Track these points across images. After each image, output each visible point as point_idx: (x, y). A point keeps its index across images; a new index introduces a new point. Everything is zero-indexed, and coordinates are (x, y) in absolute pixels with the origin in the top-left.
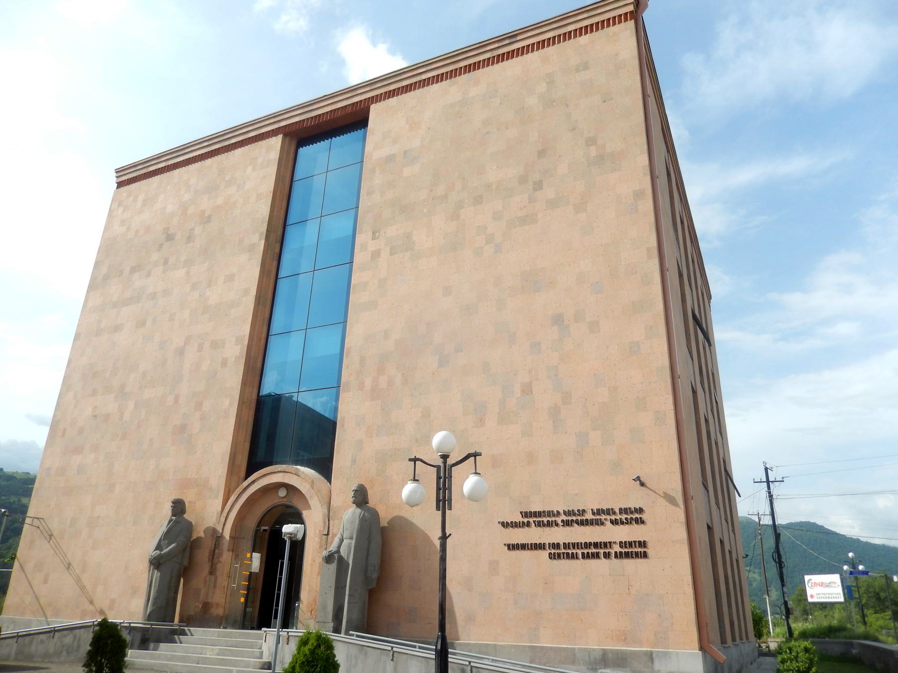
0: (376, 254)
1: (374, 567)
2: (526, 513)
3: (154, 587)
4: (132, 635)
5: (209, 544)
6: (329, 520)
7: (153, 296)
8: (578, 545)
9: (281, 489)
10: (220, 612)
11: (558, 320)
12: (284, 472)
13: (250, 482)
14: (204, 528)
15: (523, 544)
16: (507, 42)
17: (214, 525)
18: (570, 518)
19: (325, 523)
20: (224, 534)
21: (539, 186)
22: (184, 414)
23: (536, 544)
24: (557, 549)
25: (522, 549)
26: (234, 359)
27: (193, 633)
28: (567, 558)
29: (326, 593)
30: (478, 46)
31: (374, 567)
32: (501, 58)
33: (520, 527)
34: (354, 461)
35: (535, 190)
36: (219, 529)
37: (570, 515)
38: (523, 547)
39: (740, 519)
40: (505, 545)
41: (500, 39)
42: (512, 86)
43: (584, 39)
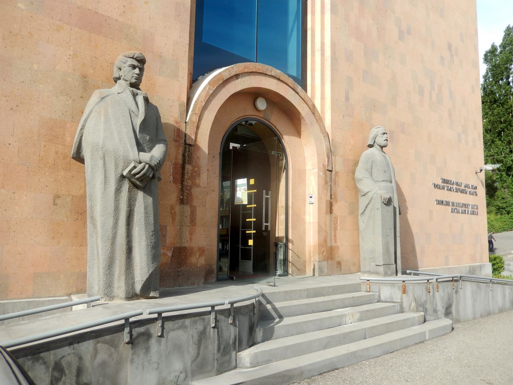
12: (279, 79)
36: (190, 132)
39: (236, 180)
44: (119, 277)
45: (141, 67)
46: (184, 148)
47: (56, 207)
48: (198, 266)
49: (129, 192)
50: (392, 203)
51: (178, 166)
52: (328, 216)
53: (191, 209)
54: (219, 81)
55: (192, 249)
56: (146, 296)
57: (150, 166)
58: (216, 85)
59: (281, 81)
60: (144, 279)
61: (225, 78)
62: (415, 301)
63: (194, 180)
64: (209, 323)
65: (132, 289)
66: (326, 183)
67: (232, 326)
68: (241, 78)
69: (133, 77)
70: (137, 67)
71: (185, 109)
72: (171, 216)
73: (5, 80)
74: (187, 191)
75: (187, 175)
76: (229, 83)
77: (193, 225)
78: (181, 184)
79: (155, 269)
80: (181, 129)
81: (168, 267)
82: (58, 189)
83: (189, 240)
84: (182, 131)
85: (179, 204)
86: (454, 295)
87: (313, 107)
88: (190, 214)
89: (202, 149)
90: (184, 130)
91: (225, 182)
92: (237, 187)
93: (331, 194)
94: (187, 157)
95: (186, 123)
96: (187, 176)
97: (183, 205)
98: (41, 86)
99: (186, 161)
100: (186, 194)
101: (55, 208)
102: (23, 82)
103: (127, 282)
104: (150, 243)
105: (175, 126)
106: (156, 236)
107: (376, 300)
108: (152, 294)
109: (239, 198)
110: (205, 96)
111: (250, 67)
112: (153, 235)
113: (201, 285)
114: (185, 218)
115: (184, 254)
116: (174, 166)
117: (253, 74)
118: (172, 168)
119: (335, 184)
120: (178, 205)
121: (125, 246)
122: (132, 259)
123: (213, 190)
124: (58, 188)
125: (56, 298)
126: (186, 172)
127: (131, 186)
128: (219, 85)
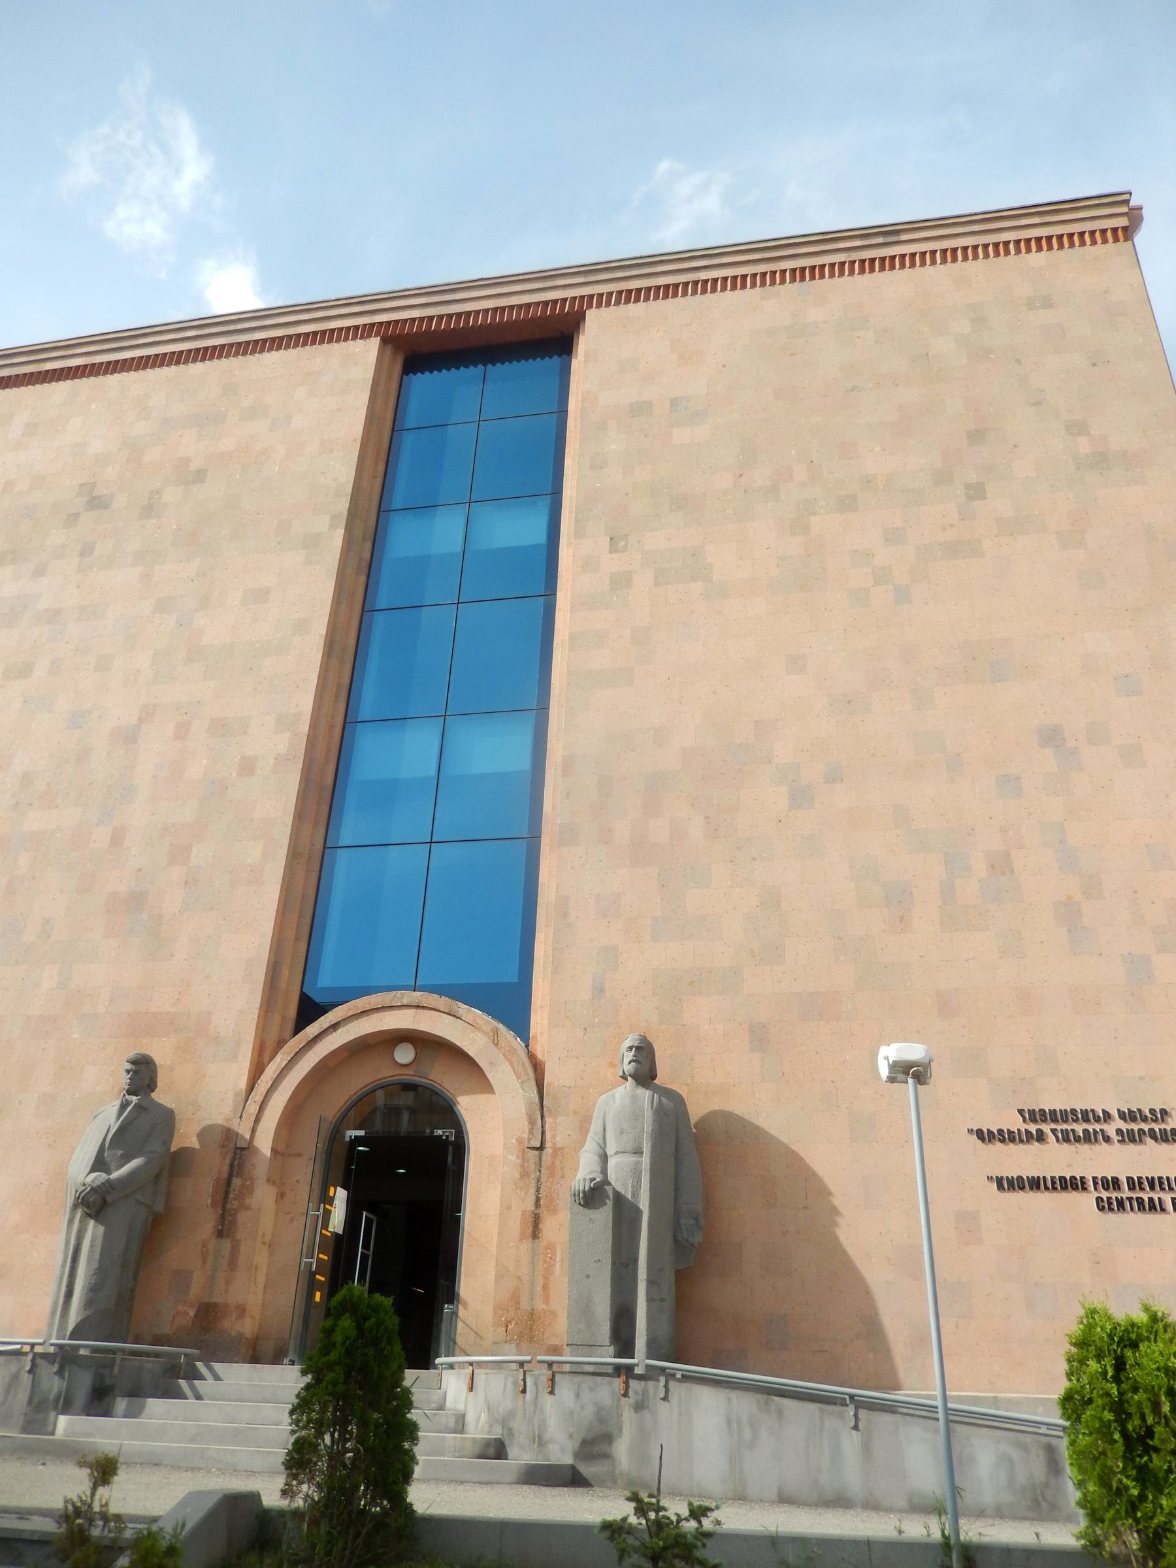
0: (621, 581)
1: (696, 1219)
2: (1032, 1113)
3: (90, 1258)
4: (66, 1377)
5: (215, 1165)
6: (542, 1117)
7: (54, 616)
8: (1161, 1183)
9: (398, 1047)
10: (247, 1327)
11: (1052, 737)
12: (418, 1007)
13: (325, 1027)
14: (201, 1127)
15: (1033, 1177)
16: (880, 240)
17: (227, 1120)
18: (1135, 1127)
19: (532, 1123)
20: (255, 1144)
21: (976, 491)
22: (139, 870)
23: (1062, 1179)
24: (1114, 1189)
25: (1031, 1189)
26: (272, 762)
27: (221, 1375)
28: (1139, 1209)
29: (588, 1277)
30: (820, 237)
31: (696, 1219)
32: (869, 266)
33: (1021, 1141)
34: (599, 990)
35: (970, 498)
36: (244, 1130)
37: (1133, 1119)
38: (1035, 1184)
40: (990, 1179)
41: (866, 233)
42: (897, 315)
43: (1036, 259)
48: (233, 1334)
50: (606, 1200)
52: (526, 1246)
55: (226, 1306)
59: (424, 1008)
61: (312, 1036)
62: (489, 1410)
64: (24, 1367)
66: (524, 1175)
67: (56, 1378)
75: (234, 1194)
86: (628, 1416)
87: (494, 1034)
93: (537, 1197)
94: (237, 1168)
96: (232, 1195)
99: (235, 1172)
107: (434, 1405)
111: (360, 1005)
117: (365, 1014)
119: (552, 1174)
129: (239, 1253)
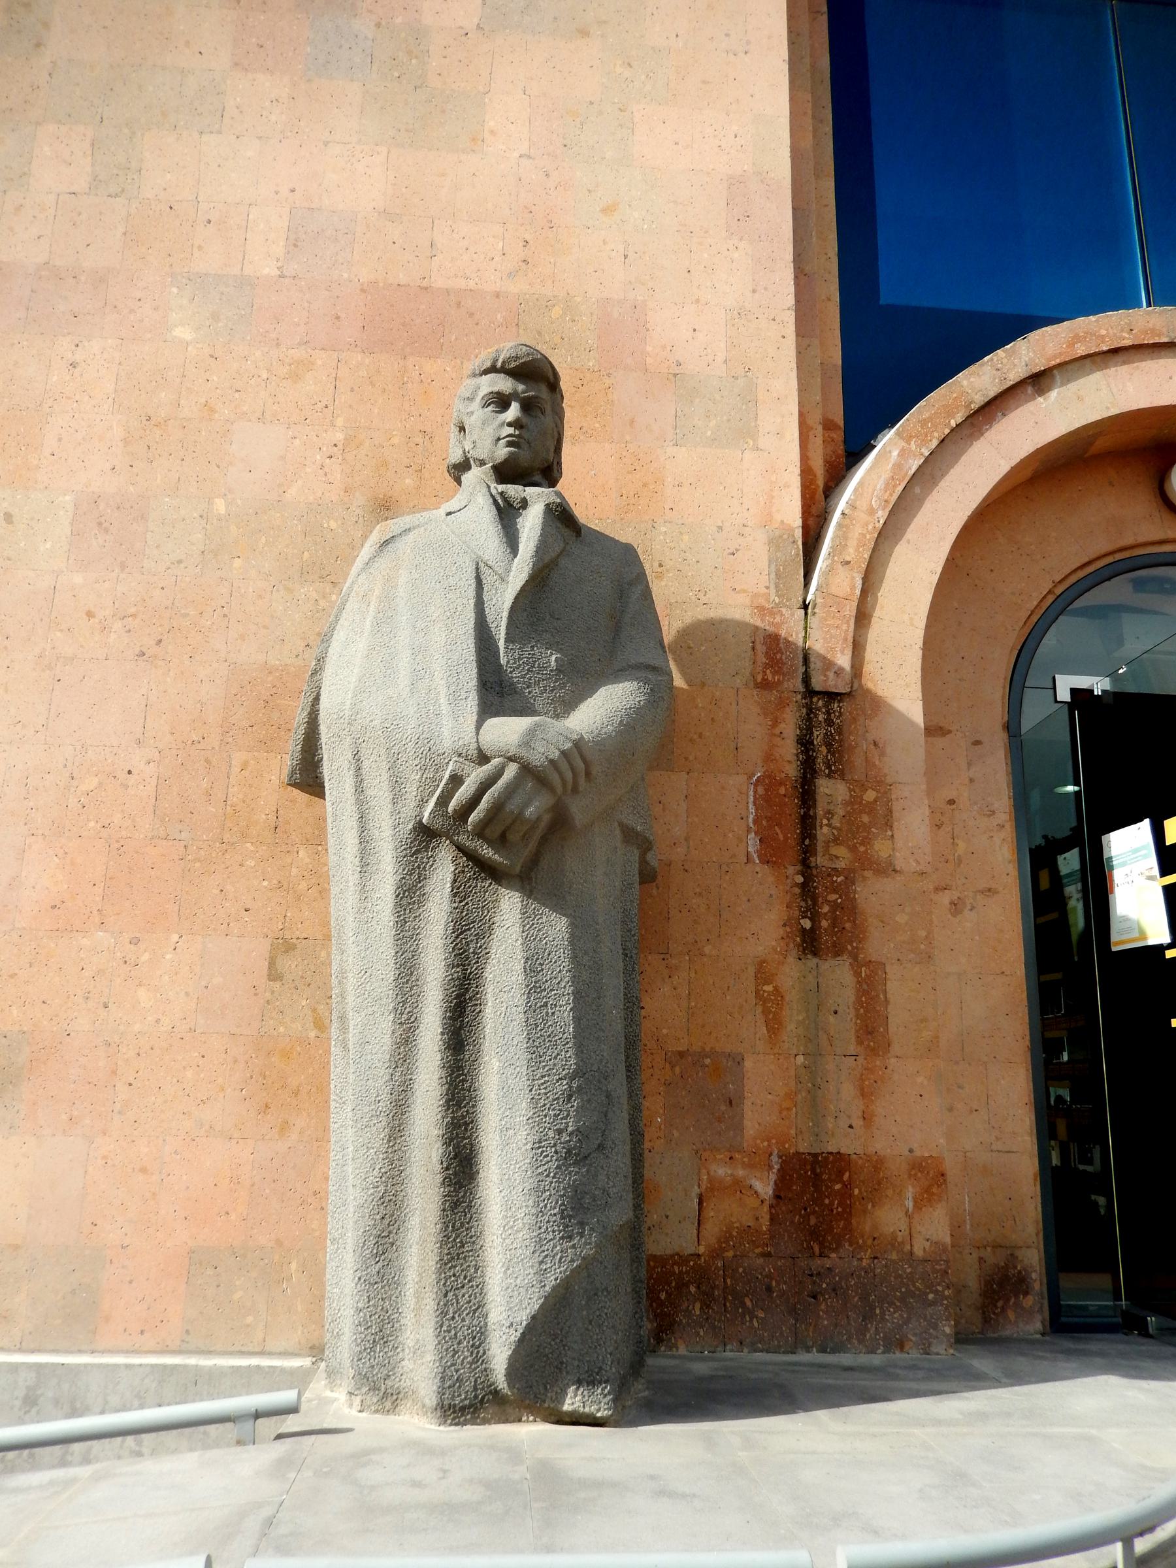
13: (1014, 376)
44: (418, 1297)
45: (531, 393)
46: (804, 711)
47: (277, 986)
49: (455, 895)
51: (782, 791)
53: (857, 974)
54: (951, 415)
55: (878, 1163)
56: (546, 1405)
57: (526, 769)
58: (936, 434)
60: (518, 1319)
61: (979, 400)
63: (862, 844)
65: (471, 1364)
68: (1062, 384)
69: (499, 439)
70: (514, 396)
71: (798, 555)
72: (759, 1010)
73: (123, 566)
74: (832, 897)
75: (829, 825)
76: (1004, 415)
77: (874, 1052)
78: (799, 867)
79: (579, 1266)
80: (783, 633)
81: (758, 1251)
82: (287, 919)
83: (857, 1122)
84: (788, 643)
85: (794, 952)
88: (852, 999)
89: (890, 706)
90: (797, 638)
91: (1063, 856)
92: (1111, 868)
94: (824, 749)
95: (805, 607)
96: (825, 830)
97: (815, 960)
98: (237, 563)
99: (820, 764)
100: (826, 909)
101: (273, 992)
102: (180, 562)
103: (445, 1328)
104: (551, 1133)
105: (757, 628)
106: (589, 1101)
108: (573, 1401)
109: (1126, 919)
110: (887, 484)
111: (1103, 332)
112: (570, 1097)
113: (942, 1350)
114: (832, 1019)
115: (838, 1187)
116: (761, 790)
117: (1120, 357)
118: (751, 799)
120: (791, 959)
121: (439, 1144)
122: (474, 1210)
123: (990, 890)
124: (288, 915)
125: (265, 1362)
126: (820, 812)
127: (463, 872)
128: (952, 430)
129: (887, 1001)
